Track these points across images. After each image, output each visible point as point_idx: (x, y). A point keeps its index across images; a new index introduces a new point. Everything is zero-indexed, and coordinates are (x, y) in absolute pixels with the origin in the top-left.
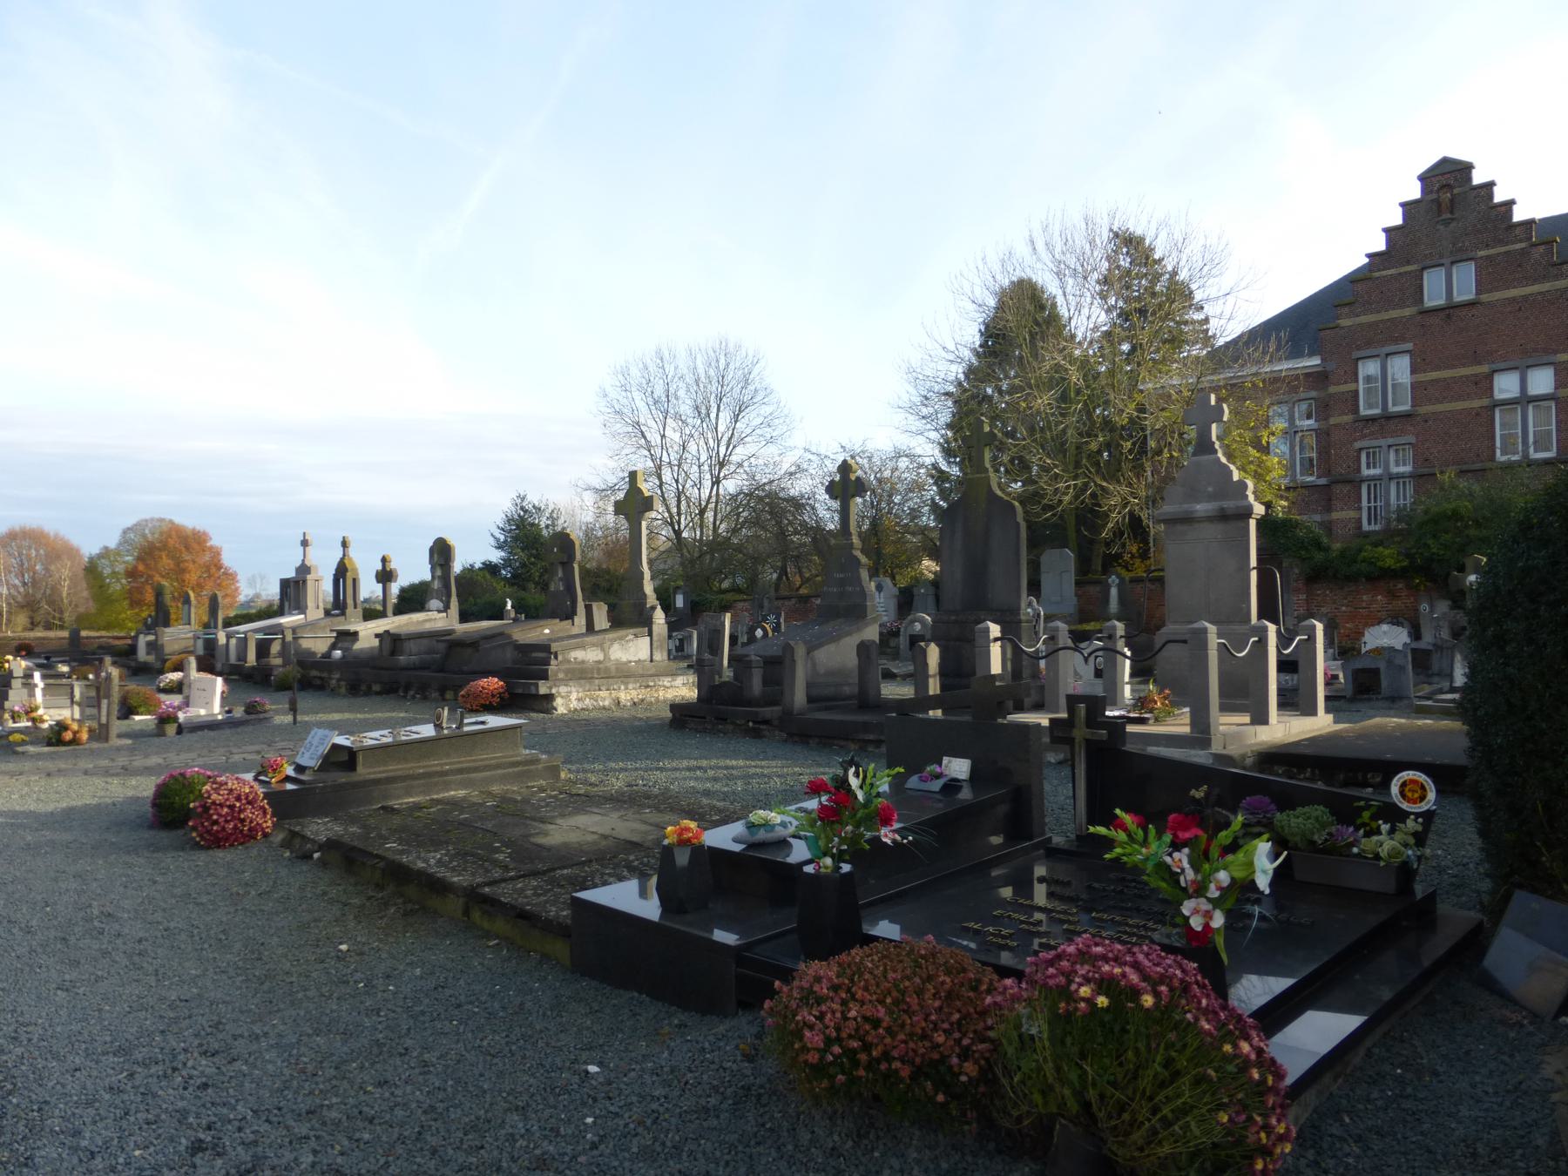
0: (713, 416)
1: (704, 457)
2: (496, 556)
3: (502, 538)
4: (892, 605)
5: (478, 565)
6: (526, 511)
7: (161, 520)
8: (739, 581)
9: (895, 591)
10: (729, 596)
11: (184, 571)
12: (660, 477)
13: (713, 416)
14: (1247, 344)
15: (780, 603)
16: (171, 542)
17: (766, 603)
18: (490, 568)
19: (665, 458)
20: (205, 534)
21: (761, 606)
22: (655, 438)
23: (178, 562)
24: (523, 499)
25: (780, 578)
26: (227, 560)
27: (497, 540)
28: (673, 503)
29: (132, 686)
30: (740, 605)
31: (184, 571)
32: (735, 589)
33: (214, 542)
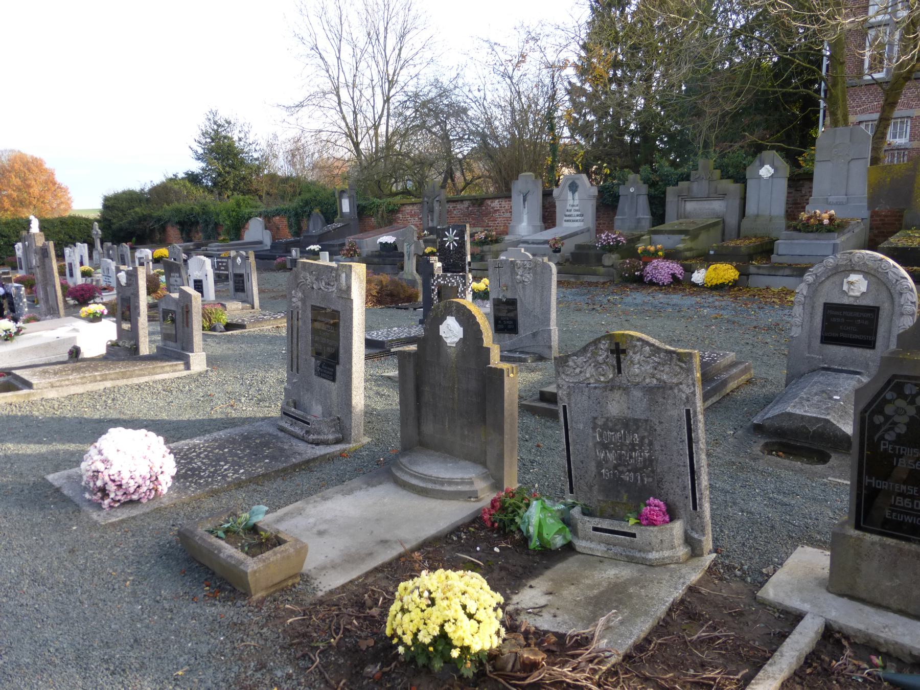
0: (382, 41)
1: (376, 78)
2: (197, 167)
3: (200, 151)
4: (590, 208)
5: (181, 175)
6: (219, 126)
7: (12, 151)
8: (410, 185)
9: (594, 191)
10: (398, 199)
11: (29, 186)
12: (338, 96)
13: (382, 41)
14: (187, 306)
15: (451, 206)
16: (17, 166)
17: (437, 207)
18: (193, 178)
19: (342, 80)
20: (41, 160)
21: (431, 211)
22: (331, 60)
23: (24, 180)
24: (215, 115)
25: (445, 180)
26: (59, 178)
27: (196, 152)
28: (350, 119)
29: (525, 168)
30: (408, 209)
31: (29, 186)
32: (406, 192)
33: (48, 166)
